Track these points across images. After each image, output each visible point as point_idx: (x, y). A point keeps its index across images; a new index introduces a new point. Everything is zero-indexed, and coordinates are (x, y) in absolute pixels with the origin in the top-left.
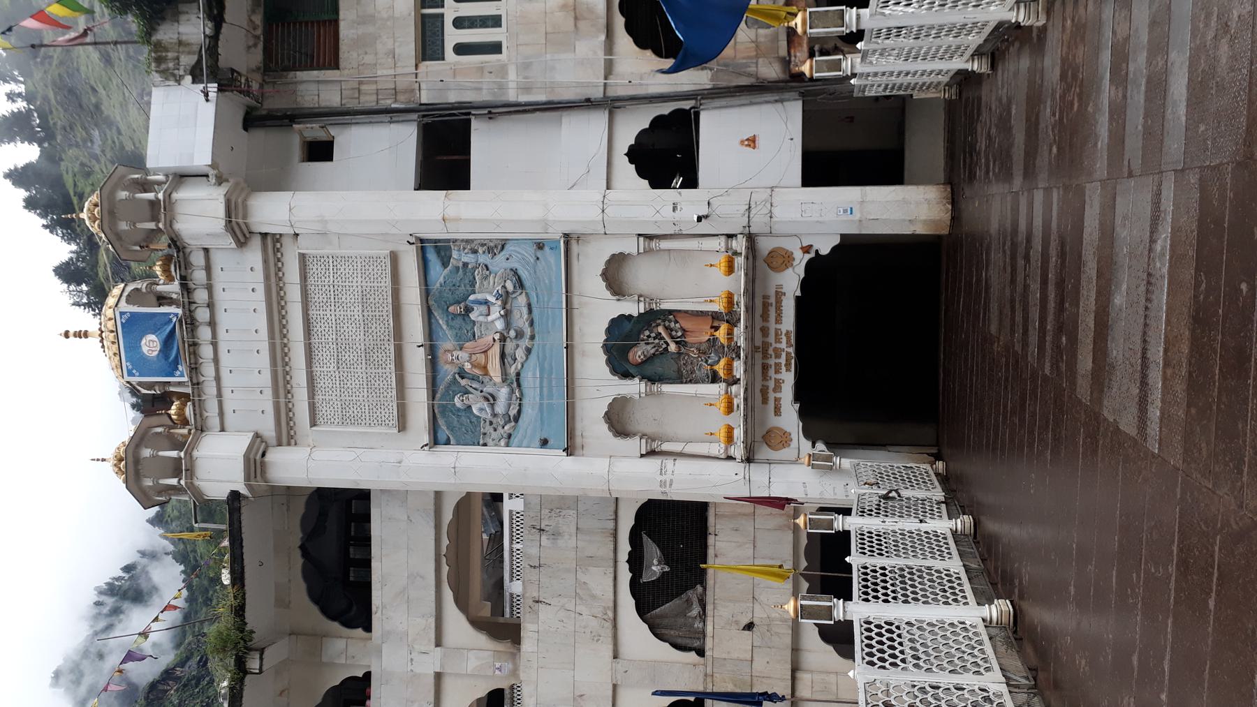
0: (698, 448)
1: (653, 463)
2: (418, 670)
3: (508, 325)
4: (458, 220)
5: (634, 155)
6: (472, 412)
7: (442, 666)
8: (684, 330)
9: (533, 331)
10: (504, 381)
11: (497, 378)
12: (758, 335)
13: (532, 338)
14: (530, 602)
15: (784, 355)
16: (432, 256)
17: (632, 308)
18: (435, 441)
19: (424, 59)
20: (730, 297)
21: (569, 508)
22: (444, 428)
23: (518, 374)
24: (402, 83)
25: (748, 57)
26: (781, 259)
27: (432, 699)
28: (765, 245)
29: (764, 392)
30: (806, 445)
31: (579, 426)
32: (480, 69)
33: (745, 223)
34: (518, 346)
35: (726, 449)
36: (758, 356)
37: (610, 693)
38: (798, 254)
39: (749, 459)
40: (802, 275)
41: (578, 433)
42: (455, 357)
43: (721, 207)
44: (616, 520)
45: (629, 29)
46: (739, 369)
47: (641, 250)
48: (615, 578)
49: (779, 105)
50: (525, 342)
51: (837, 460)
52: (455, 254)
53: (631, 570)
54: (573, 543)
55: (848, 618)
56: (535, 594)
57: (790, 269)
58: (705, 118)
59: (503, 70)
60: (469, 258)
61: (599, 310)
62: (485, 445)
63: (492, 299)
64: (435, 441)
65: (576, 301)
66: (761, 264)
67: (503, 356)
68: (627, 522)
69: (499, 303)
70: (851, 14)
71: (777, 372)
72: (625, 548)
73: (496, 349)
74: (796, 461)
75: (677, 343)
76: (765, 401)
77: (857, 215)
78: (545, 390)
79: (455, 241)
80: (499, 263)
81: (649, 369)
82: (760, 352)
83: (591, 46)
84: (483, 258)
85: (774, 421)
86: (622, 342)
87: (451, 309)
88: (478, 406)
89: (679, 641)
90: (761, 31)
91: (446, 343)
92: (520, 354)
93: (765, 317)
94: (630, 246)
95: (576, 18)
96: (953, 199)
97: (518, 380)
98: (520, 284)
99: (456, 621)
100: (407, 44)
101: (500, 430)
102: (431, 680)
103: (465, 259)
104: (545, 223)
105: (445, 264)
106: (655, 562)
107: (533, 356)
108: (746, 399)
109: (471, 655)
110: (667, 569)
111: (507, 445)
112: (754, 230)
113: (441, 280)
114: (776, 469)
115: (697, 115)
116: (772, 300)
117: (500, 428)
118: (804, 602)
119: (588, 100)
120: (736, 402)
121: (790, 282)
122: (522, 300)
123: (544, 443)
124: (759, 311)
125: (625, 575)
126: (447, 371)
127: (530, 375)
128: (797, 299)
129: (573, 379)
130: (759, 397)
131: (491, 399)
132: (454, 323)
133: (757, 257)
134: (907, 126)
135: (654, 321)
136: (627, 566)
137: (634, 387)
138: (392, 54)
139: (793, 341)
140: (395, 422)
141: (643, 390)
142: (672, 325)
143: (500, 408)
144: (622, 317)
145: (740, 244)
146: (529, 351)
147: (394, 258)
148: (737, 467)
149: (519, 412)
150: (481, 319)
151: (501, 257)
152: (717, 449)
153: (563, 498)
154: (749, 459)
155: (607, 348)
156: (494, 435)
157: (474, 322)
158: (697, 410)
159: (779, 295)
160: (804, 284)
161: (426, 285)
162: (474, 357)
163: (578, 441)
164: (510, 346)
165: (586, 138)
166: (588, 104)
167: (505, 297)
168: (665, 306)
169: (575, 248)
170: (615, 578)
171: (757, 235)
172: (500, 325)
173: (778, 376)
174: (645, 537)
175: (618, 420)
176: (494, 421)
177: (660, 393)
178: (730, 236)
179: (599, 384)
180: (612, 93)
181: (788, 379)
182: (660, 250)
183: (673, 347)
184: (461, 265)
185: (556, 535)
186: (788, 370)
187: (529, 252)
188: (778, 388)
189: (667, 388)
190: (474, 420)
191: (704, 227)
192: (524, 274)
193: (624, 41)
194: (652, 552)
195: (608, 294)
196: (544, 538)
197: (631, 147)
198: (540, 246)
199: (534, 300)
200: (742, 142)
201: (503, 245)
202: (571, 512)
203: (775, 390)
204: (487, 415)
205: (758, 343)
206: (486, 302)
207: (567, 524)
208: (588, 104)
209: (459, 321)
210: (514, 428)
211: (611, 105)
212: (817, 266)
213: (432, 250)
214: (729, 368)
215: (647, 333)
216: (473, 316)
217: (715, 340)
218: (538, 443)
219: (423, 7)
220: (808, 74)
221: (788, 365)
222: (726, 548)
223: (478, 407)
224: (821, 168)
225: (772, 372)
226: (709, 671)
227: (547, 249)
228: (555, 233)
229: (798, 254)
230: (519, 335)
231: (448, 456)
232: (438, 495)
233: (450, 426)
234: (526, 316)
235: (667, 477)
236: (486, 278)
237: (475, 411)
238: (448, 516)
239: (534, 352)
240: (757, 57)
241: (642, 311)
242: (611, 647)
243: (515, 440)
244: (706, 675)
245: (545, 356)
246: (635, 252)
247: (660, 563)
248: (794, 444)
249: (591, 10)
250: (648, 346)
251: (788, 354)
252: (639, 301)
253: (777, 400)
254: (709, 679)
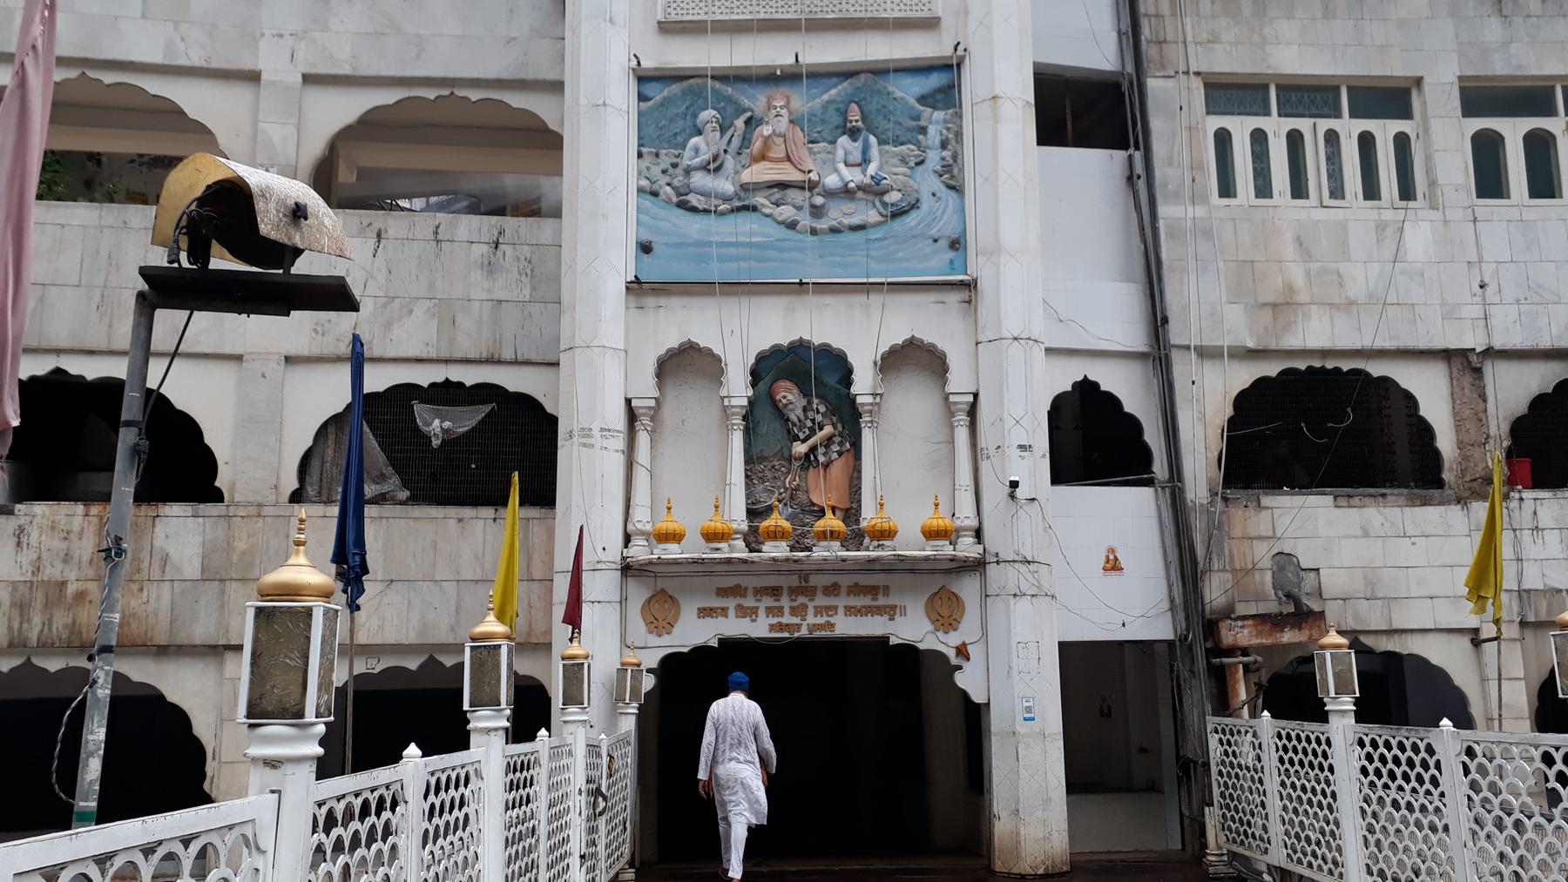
0: (645, 485)
1: (618, 420)
2: (263, 45)
3: (830, 194)
4: (996, 120)
5: (1086, 388)
6: (692, 136)
7: (272, 83)
8: (826, 466)
9: (823, 232)
10: (745, 187)
11: (747, 176)
12: (828, 580)
13: (814, 232)
14: (378, 225)
15: (796, 620)
16: (935, 80)
17: (863, 383)
18: (644, 78)
19: (1206, 85)
20: (887, 534)
21: (533, 289)
22: (665, 93)
23: (755, 209)
24: (1173, 52)
25: (1232, 561)
26: (945, 612)
27: (215, 65)
28: (968, 589)
29: (737, 591)
30: (652, 659)
31: (675, 302)
32: (1197, 166)
33: (1003, 556)
34: (799, 208)
35: (642, 533)
36: (794, 581)
37: (228, 350)
38: (954, 639)
39: (627, 569)
40: (921, 646)
41: (663, 301)
42: (779, 113)
43: (1029, 514)
44: (516, 362)
45: (1261, 383)
46: (776, 550)
47: (952, 398)
48: (419, 360)
49: (1166, 605)
50: (805, 220)
51: (633, 709)
52: (939, 115)
53: (433, 385)
54: (477, 294)
55: (474, 738)
56: (391, 233)
57: (930, 627)
58: (1144, 494)
59: (1197, 198)
60: (933, 136)
61: (860, 334)
62: (640, 155)
63: (872, 169)
64: (644, 78)
65: (876, 299)
66: (939, 581)
67: (783, 186)
68: (512, 380)
69: (867, 180)
70: (1347, 703)
71: (769, 610)
72: (470, 376)
73: (795, 176)
74: (625, 644)
75: (807, 455)
76: (722, 592)
77: (1022, 728)
78: (733, 251)
79: (959, 115)
80: (927, 183)
81: (764, 413)
82: (800, 582)
83: (1238, 328)
84: (934, 158)
85: (689, 611)
86: (808, 371)
87: (854, 106)
88: (703, 146)
89: (315, 463)
90: (1268, 577)
91: (801, 100)
92: (786, 212)
93: (855, 590)
94: (959, 381)
95: (1274, 306)
96: (1051, 876)
97: (746, 208)
98: (898, 213)
99: (347, 108)
100: (1229, 61)
101: (663, 180)
102: (247, 65)
103: (932, 130)
104: (995, 251)
105: (922, 100)
106: (447, 424)
107: (784, 233)
108: (729, 561)
109: (291, 130)
110: (436, 443)
111: (640, 190)
112: (992, 570)
113: (899, 94)
114: (613, 612)
115: (1149, 483)
116: (882, 601)
117: (667, 179)
118: (504, 651)
119: (1165, 320)
120: (723, 545)
121: (911, 627)
122: (873, 216)
123: (645, 248)
124: (865, 580)
125: (424, 376)
126: (756, 99)
127: (755, 227)
128: (885, 639)
129: (750, 293)
130: (725, 582)
131: (714, 166)
132: (832, 112)
133: (949, 576)
134: (1098, 797)
135: (841, 420)
136: (440, 379)
137: (738, 388)
138: (1214, 39)
139: (817, 634)
140: (673, 18)
141: (734, 402)
142: (835, 448)
143: (699, 180)
144: (848, 371)
145: (967, 548)
146: (792, 225)
147: (930, 24)
148: (614, 551)
149: (694, 210)
150: (840, 153)
151: (936, 184)
152: (642, 518)
153: (556, 279)
154: (627, 569)
155: (800, 346)
156: (656, 171)
157: (833, 142)
158: (704, 488)
159: (890, 611)
160: (909, 650)
161: (896, 71)
162: (780, 141)
163: (651, 301)
164: (796, 196)
165: (1114, 320)
166: (1158, 321)
167: (875, 190)
168: (867, 435)
169: (954, 298)
170: (419, 360)
171: (983, 574)
172: (832, 181)
173: (762, 613)
174: (487, 408)
175: (685, 364)
176: (679, 171)
177: (727, 430)
178: (978, 534)
179: (741, 334)
180: (1175, 356)
181: (759, 628)
182: (952, 428)
183: (800, 448)
184: (923, 123)
185: (490, 268)
186: (772, 628)
187: (946, 227)
188: (743, 612)
189: (737, 439)
190: (679, 139)
191: (994, 493)
192: (911, 219)
193: (1243, 376)
194: (465, 420)
195: (884, 348)
196: (485, 248)
197: (1095, 385)
198: (956, 244)
199: (874, 234)
200: (1112, 550)
201: (956, 188)
202: (527, 292)
203: (739, 607)
204: (687, 160)
205: (815, 580)
206: (865, 161)
207: (509, 285)
208: (1158, 321)
209: (838, 120)
210: (668, 201)
211: (1158, 355)
212: (907, 664)
213: (945, 79)
214: (776, 535)
215: (822, 409)
216: (844, 140)
217: (821, 513)
218: (646, 237)
219: (1278, 87)
220: (1326, 640)
221: (781, 627)
222: (471, 538)
223: (702, 146)
224: (1084, 665)
225: (768, 601)
226: (267, 511)
227: (951, 254)
228: (978, 267)
229: (954, 639)
230: (817, 212)
231: (622, 95)
232: (557, 87)
233: (668, 101)
234: (846, 221)
235: (597, 439)
236: (904, 161)
237: (694, 141)
238: (516, 100)
239: (789, 233)
240: (1233, 571)
241: (859, 400)
242: (305, 352)
243: (648, 202)
244: (260, 505)
245: (782, 250)
246: (950, 388)
247: (445, 431)
248: (653, 640)
249: (1287, 327)
250: (805, 403)
251: (799, 626)
252: (875, 395)
253: (724, 612)
254: (253, 510)
